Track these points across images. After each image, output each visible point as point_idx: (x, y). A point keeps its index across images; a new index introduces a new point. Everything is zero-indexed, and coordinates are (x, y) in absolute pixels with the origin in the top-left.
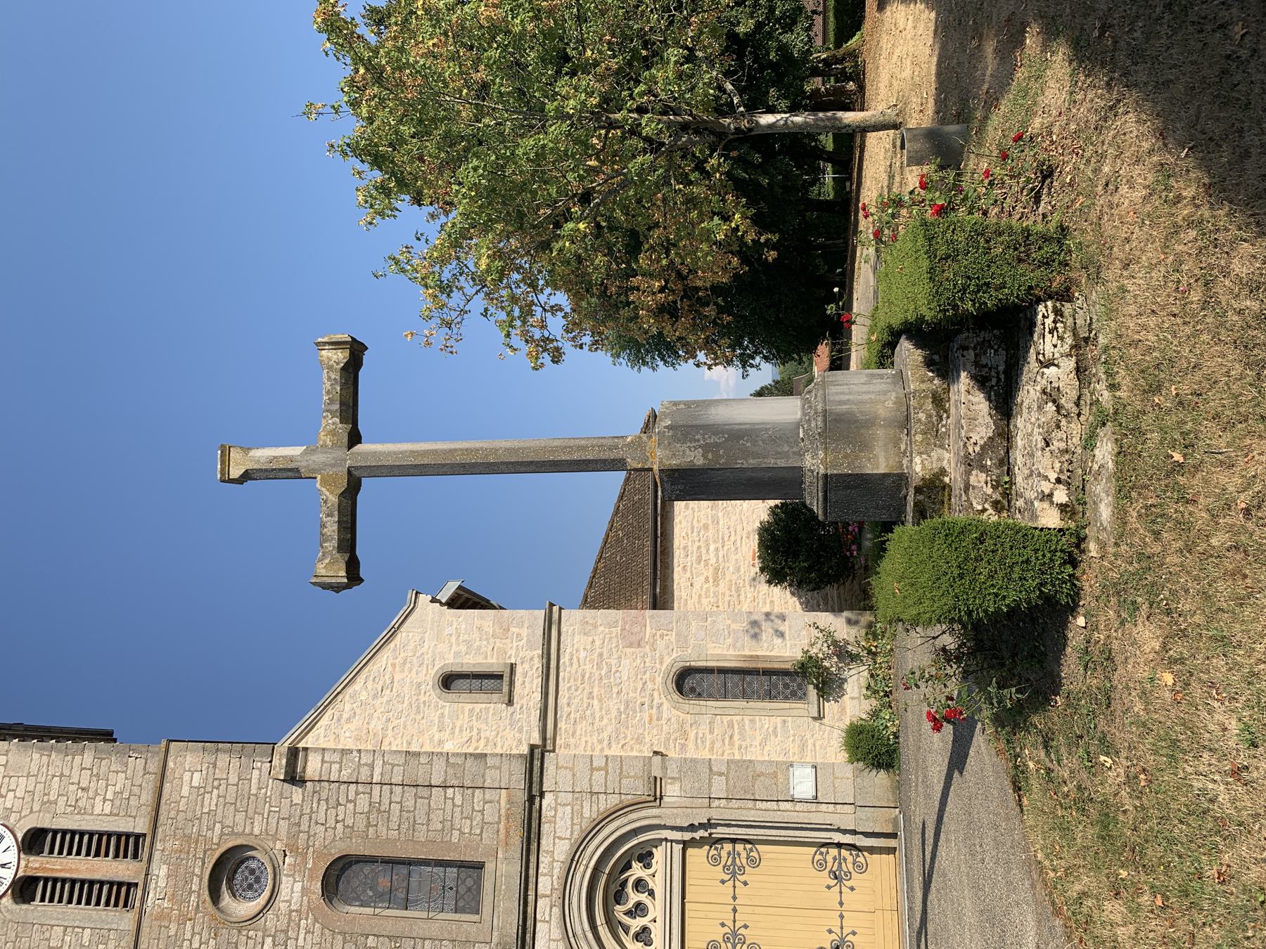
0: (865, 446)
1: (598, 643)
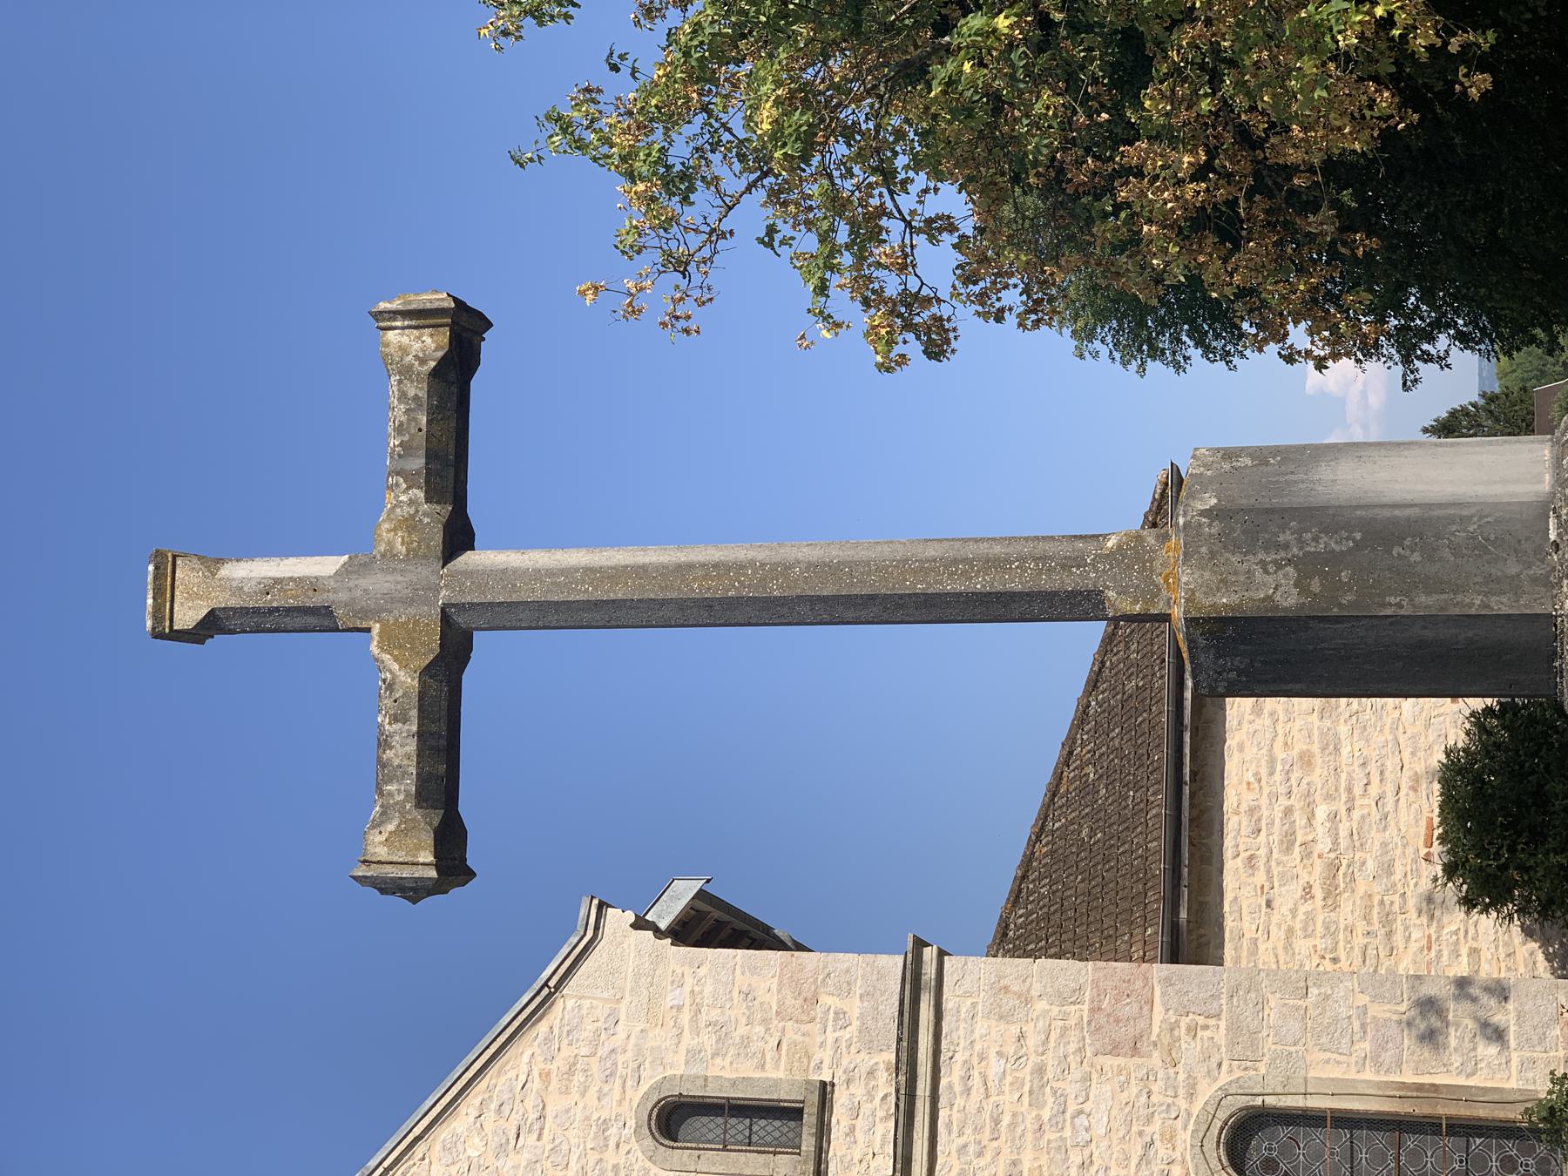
1: (1032, 1041)
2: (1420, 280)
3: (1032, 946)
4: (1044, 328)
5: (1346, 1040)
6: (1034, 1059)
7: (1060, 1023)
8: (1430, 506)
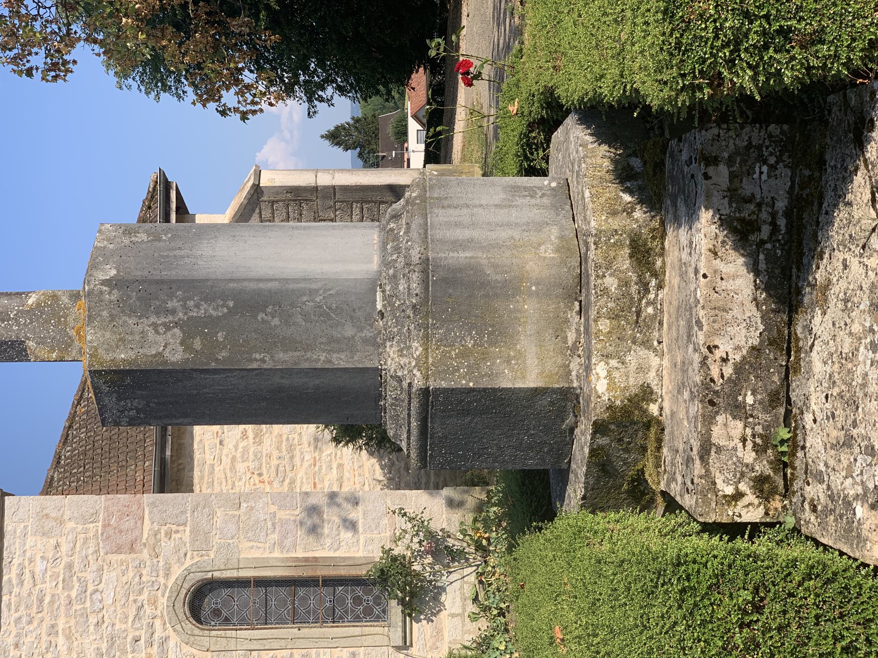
0: (499, 332)
1: (64, 548)
2: (317, 53)
3: (75, 471)
4: (60, 81)
5: (264, 533)
6: (65, 560)
7: (83, 535)
8: (287, 280)
